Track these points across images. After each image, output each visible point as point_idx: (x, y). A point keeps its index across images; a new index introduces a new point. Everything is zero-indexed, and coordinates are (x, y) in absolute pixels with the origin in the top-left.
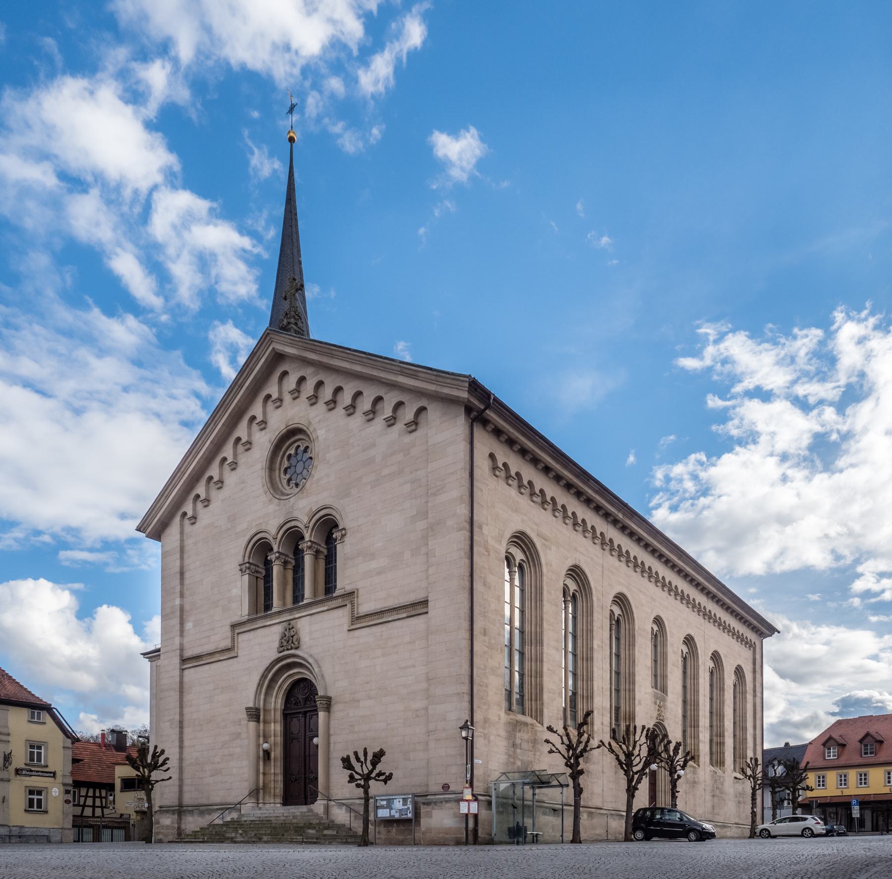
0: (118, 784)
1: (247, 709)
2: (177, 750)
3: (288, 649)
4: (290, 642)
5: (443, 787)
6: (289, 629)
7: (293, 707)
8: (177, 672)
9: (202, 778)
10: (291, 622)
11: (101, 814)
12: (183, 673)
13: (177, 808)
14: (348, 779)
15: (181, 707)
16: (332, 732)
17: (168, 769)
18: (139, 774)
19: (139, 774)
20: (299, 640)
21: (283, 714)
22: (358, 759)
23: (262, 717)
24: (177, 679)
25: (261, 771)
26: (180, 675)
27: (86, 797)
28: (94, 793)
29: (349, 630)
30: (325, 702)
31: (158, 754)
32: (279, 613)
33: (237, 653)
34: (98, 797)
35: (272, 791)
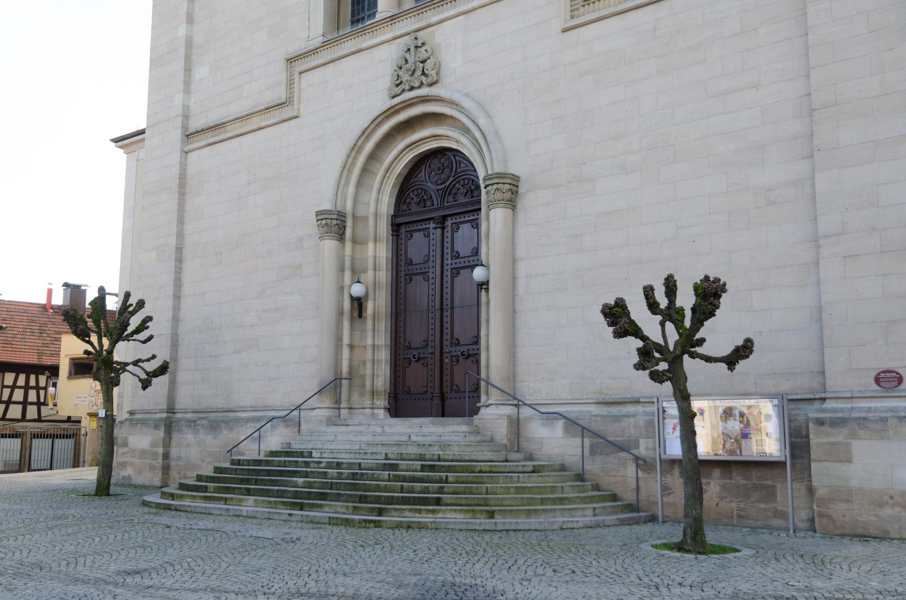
0: (64, 368)
1: (319, 213)
2: (170, 302)
3: (412, 88)
4: (419, 73)
5: (877, 380)
6: (417, 47)
7: (415, 208)
8: (176, 157)
9: (216, 356)
10: (419, 34)
11: (36, 417)
12: (186, 159)
13: (165, 415)
14: (636, 359)
15: (181, 221)
16: (521, 252)
17: (150, 338)
18: (90, 349)
19: (90, 349)
20: (438, 68)
21: (392, 225)
22: (653, 306)
23: (349, 232)
24: (176, 171)
25: (346, 340)
26: (181, 163)
27: (13, 387)
28: (27, 380)
29: (565, 31)
30: (508, 187)
31: (131, 309)
32: (393, 18)
33: (299, 110)
34: (32, 388)
35: (368, 383)
